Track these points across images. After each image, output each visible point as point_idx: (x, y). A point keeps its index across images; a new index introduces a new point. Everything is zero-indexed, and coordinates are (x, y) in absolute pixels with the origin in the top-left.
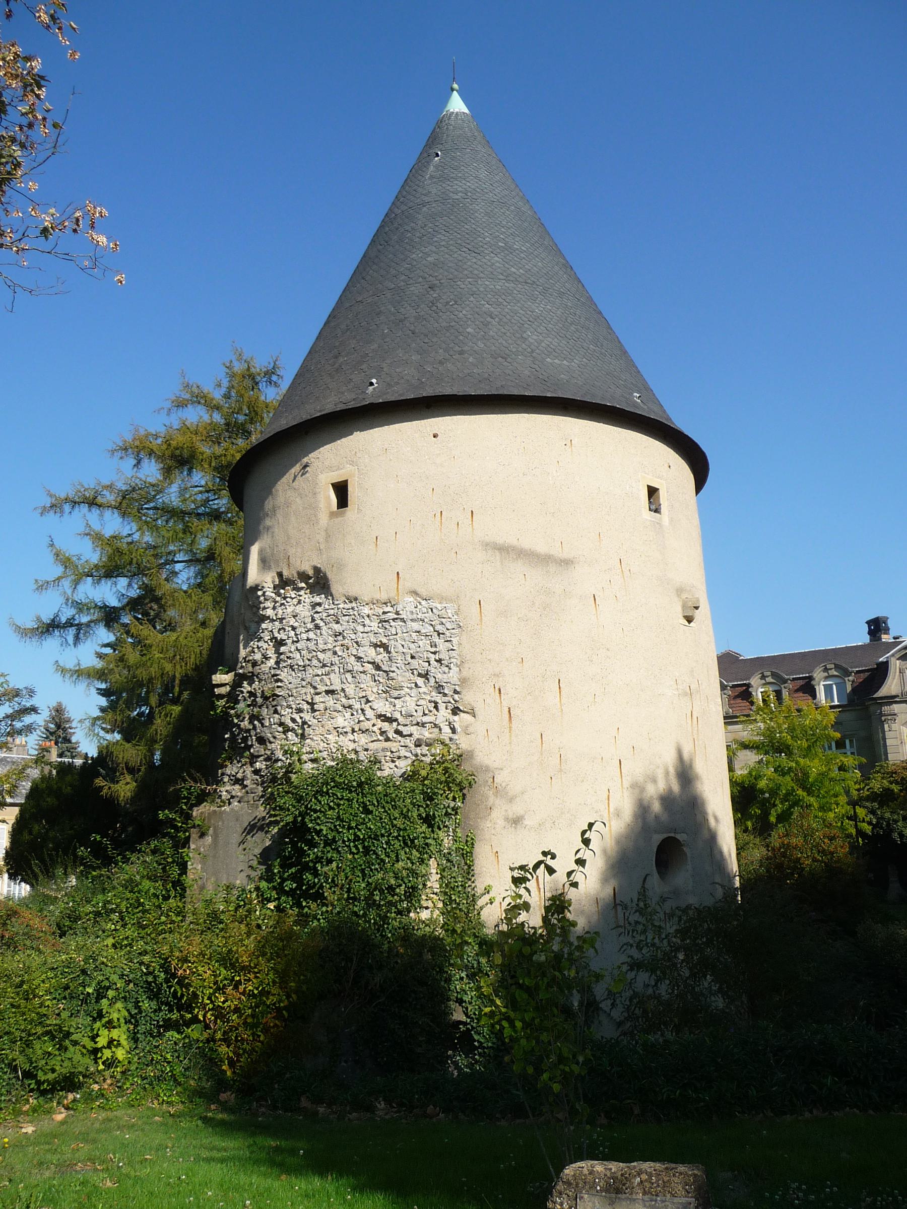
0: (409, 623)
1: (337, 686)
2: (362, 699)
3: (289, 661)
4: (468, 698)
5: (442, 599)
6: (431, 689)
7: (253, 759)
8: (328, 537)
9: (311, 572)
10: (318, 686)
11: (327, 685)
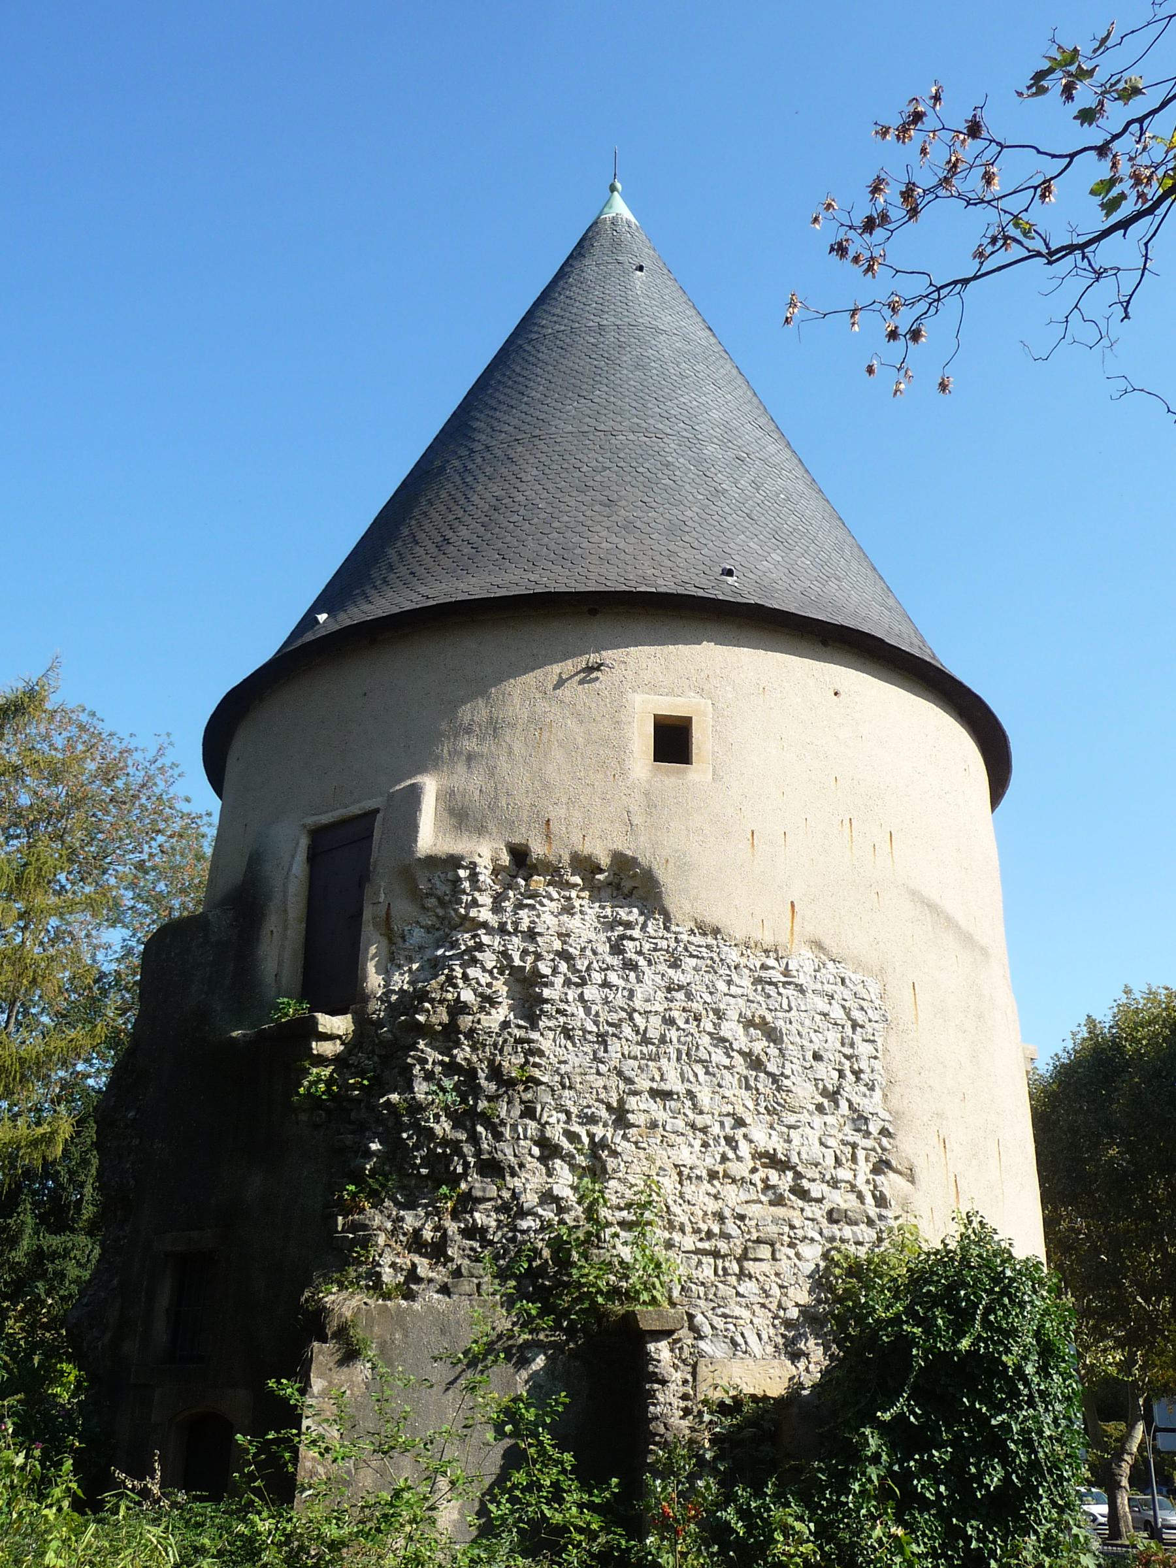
0: (809, 994)
1: (673, 1083)
2: (725, 1119)
3: (562, 1019)
4: (906, 1148)
5: (859, 966)
6: (842, 1120)
7: (467, 1202)
8: (651, 807)
9: (605, 861)
10: (636, 1079)
11: (653, 1080)
